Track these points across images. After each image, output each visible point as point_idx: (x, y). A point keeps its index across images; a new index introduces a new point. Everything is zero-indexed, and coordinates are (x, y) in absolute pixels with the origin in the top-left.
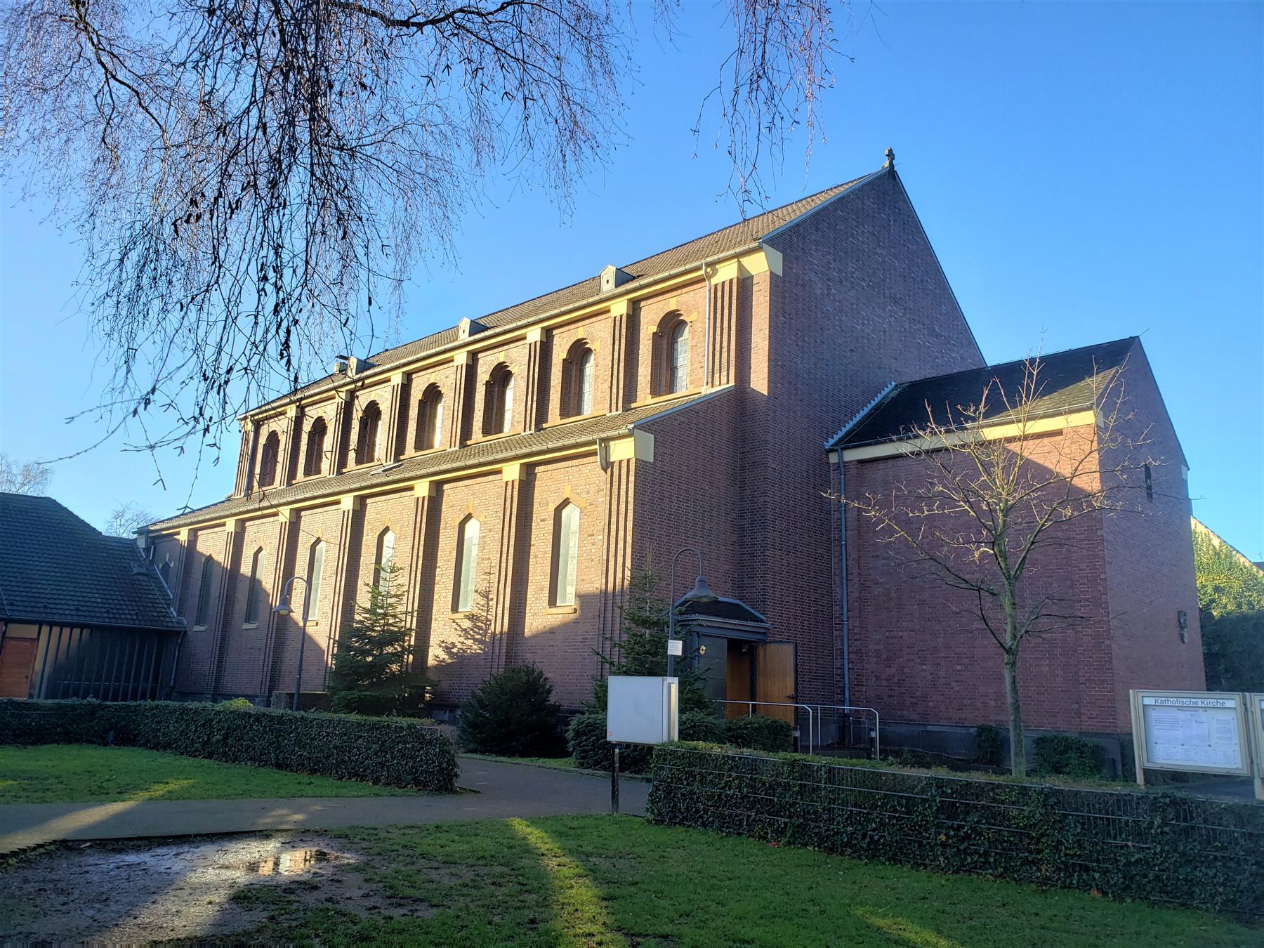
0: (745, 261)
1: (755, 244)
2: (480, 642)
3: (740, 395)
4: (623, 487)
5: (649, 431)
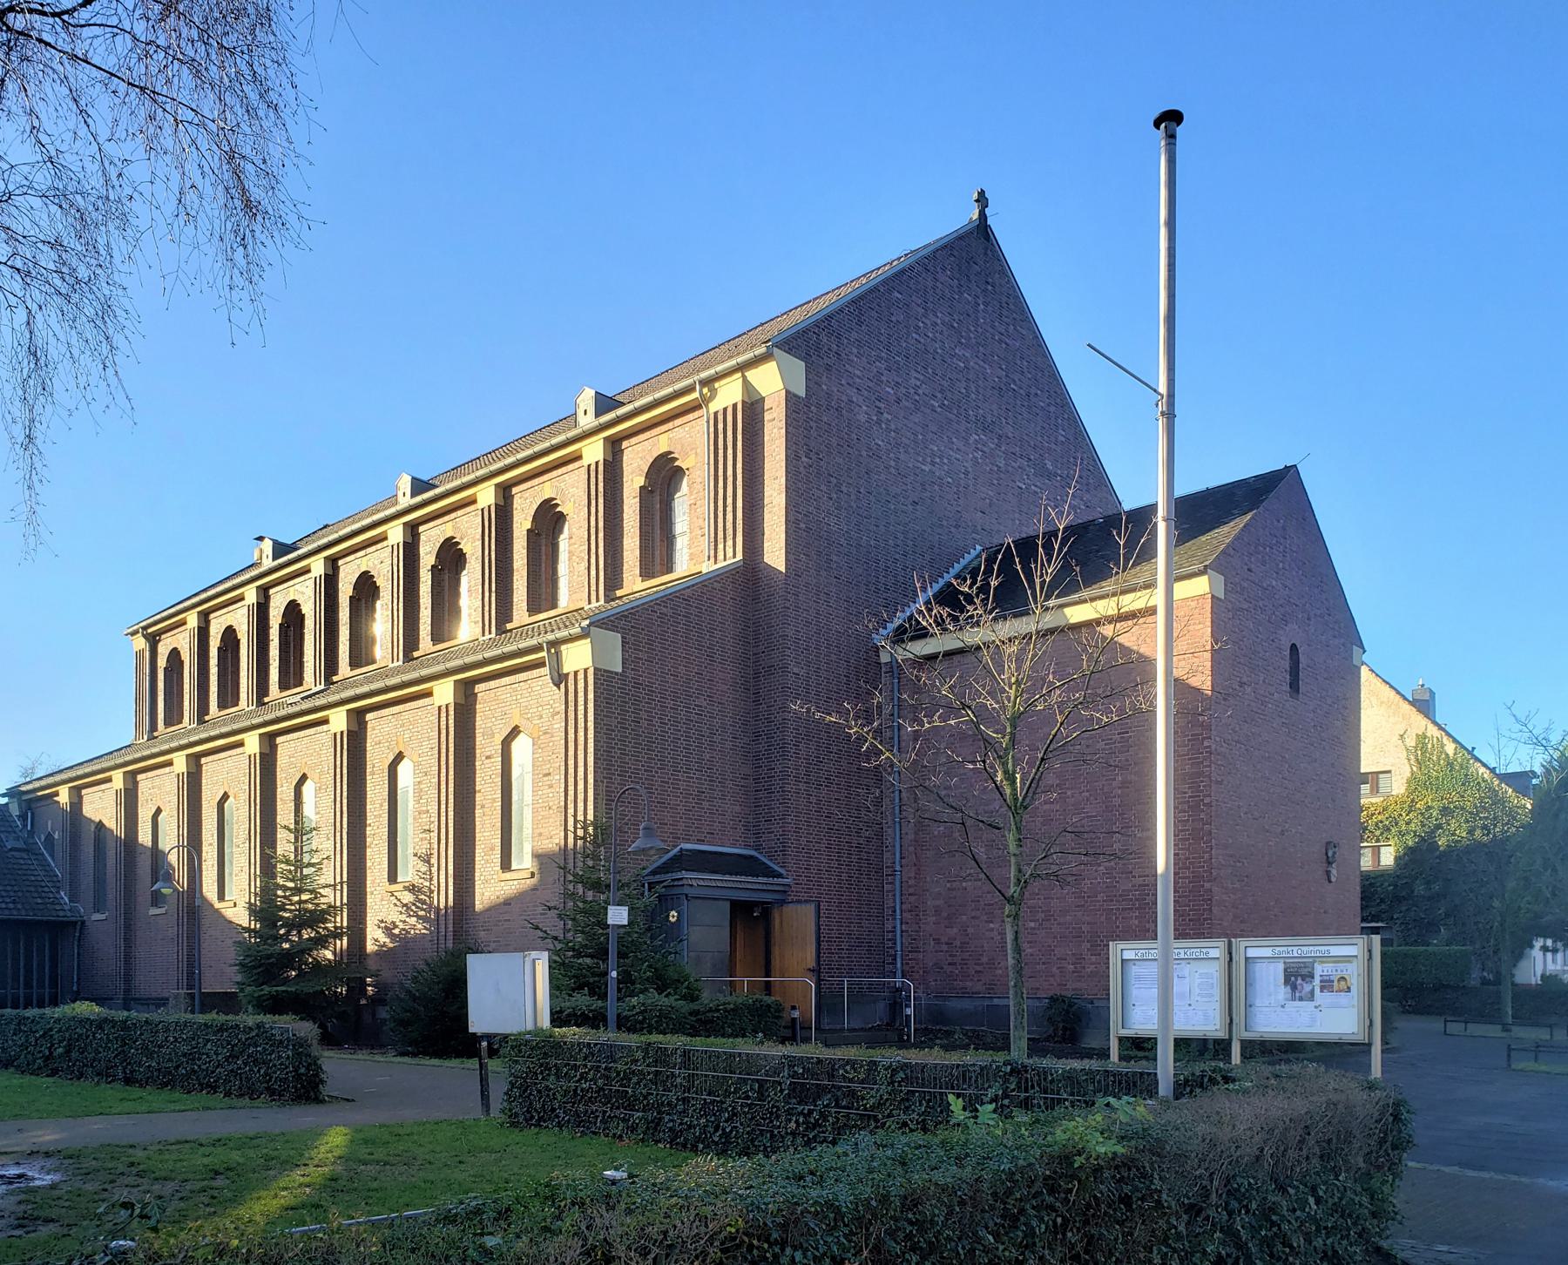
0: (750, 374)
1: (762, 350)
2: (424, 919)
3: (751, 568)
4: (581, 708)
5: (614, 629)
